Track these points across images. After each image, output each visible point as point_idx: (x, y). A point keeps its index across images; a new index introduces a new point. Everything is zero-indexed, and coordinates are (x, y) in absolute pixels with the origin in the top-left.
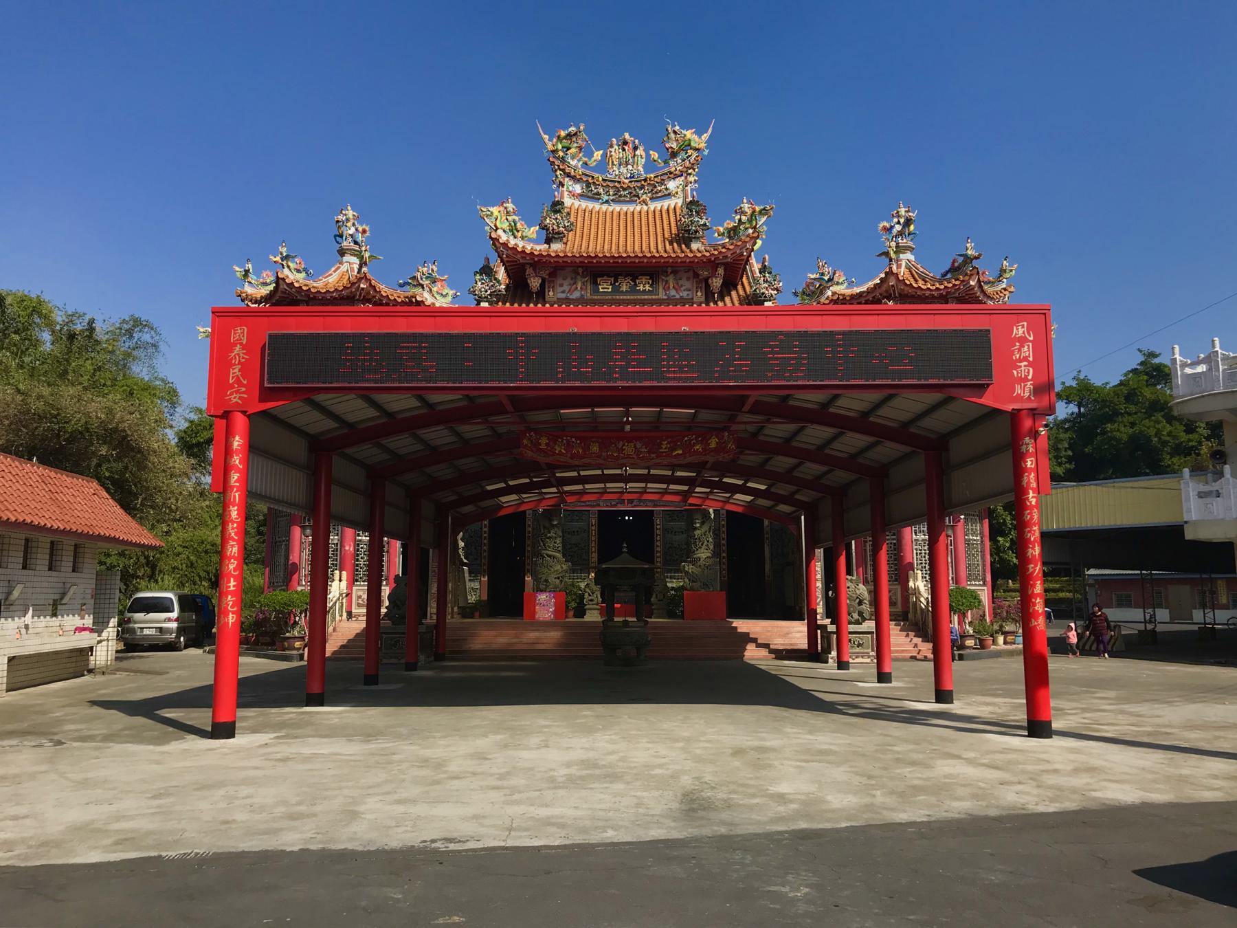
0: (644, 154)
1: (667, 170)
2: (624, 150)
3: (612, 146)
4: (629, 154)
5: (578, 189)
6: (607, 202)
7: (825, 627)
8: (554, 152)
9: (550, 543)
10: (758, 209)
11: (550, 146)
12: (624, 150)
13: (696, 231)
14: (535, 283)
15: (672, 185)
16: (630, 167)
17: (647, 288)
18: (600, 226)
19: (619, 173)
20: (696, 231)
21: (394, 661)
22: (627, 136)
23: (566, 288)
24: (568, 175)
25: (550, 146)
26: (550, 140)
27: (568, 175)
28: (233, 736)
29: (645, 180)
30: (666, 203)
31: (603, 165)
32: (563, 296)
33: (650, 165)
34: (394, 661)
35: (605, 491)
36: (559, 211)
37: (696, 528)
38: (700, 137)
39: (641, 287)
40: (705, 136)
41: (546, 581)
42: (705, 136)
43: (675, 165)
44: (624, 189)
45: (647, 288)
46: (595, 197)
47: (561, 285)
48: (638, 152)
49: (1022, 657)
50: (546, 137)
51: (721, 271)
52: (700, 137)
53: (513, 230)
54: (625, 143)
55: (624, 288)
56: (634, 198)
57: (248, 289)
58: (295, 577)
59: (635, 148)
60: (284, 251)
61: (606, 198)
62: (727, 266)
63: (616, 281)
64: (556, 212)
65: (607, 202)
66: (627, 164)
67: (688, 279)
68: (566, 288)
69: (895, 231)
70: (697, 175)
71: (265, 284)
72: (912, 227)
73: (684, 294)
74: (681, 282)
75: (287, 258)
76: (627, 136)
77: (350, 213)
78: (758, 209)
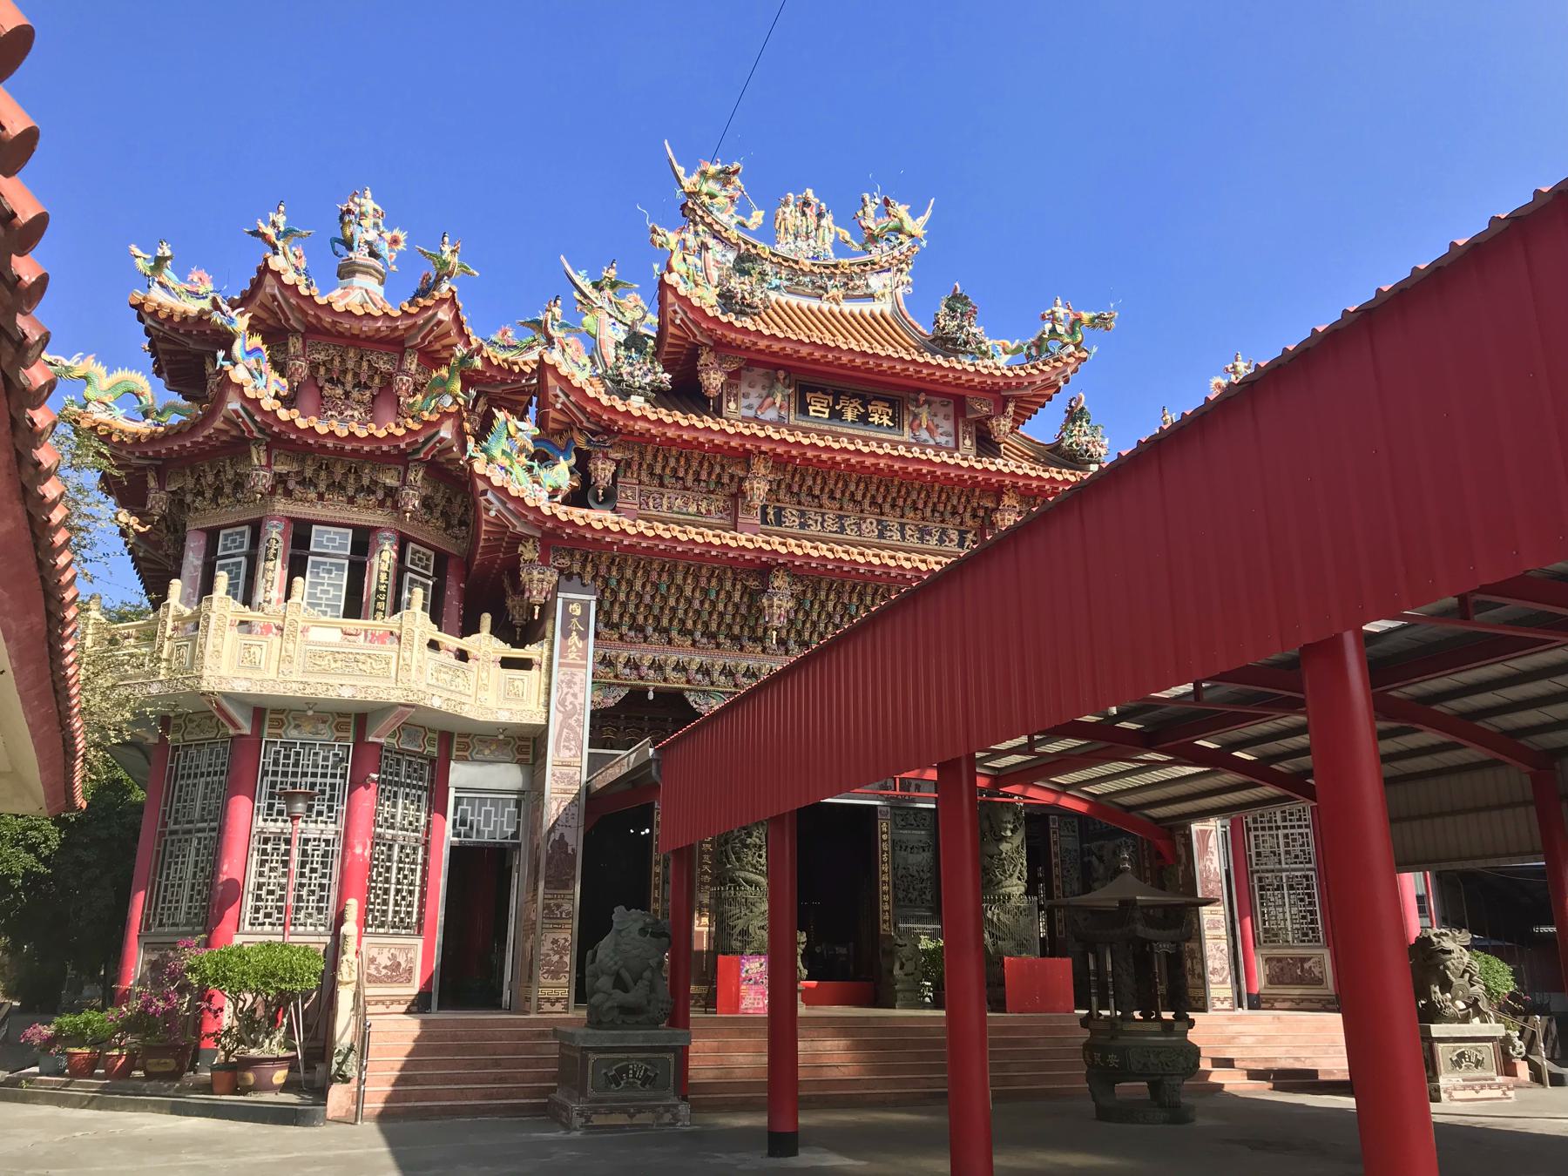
1: (866, 258)
2: (804, 214)
3: (786, 204)
4: (812, 221)
6: (777, 288)
7: (1520, 1038)
9: (749, 857)
10: (1086, 316)
12: (804, 214)
13: (966, 343)
14: (714, 380)
15: (876, 282)
16: (811, 242)
20: (966, 343)
21: (621, 1119)
22: (810, 193)
25: (688, 184)
26: (687, 175)
29: (836, 266)
30: (867, 307)
31: (768, 232)
32: (751, 413)
33: (840, 246)
34: (621, 1119)
37: (1004, 839)
38: (914, 218)
39: (876, 419)
40: (922, 220)
41: (745, 932)
42: (922, 220)
43: (878, 253)
44: (805, 274)
45: (886, 421)
47: (746, 396)
48: (824, 222)
49: (763, 1041)
52: (914, 218)
54: (806, 203)
55: (849, 415)
56: (819, 292)
57: (157, 295)
58: (231, 913)
59: (820, 215)
61: (776, 282)
63: (836, 402)
65: (777, 288)
67: (946, 417)
68: (755, 402)
70: (910, 274)
71: (196, 295)
74: (936, 421)
77: (369, 205)
78: (1086, 316)
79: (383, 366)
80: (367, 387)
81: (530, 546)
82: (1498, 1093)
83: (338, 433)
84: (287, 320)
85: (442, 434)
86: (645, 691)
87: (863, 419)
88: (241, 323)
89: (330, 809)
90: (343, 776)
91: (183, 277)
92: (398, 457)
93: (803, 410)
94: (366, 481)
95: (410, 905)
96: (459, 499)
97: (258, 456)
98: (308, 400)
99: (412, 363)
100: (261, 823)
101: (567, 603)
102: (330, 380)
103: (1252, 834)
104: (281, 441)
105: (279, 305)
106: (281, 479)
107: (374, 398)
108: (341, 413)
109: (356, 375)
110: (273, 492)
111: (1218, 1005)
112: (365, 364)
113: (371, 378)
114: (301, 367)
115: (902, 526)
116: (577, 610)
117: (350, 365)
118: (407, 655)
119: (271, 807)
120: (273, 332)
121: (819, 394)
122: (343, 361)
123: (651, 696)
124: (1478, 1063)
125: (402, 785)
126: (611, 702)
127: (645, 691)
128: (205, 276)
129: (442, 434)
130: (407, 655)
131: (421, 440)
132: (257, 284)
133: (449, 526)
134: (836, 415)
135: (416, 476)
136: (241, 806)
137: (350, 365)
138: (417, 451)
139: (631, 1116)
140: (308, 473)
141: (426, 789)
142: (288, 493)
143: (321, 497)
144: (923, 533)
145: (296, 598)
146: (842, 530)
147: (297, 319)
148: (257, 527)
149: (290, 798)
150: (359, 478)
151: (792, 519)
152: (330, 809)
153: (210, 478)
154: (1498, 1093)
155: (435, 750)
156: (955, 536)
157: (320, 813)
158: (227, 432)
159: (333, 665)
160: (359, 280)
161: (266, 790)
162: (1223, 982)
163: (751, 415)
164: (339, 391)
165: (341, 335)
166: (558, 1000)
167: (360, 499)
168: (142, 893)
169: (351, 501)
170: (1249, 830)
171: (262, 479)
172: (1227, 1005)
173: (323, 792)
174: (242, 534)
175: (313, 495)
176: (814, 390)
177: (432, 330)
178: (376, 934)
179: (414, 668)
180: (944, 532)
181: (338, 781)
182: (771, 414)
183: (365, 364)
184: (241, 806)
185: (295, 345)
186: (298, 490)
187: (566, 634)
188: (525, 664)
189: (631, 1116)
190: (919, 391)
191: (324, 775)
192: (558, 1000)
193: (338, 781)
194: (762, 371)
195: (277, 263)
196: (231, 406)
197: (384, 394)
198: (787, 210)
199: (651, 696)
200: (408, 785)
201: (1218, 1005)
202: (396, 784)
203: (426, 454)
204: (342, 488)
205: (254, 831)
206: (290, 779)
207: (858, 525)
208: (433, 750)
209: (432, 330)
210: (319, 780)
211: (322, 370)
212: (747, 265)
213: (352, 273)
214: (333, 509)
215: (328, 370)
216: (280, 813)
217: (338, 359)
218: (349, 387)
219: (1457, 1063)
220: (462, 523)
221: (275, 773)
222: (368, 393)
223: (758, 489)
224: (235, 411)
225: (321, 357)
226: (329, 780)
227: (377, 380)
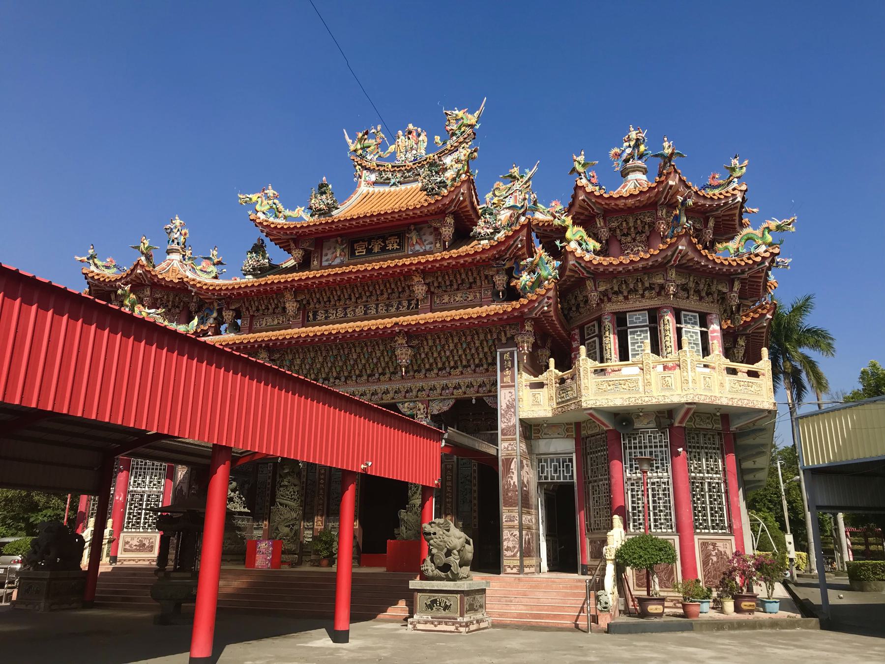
0: (426, 140)
2: (409, 138)
4: (412, 142)
5: (373, 177)
6: (394, 184)
8: (355, 151)
11: (352, 148)
12: (409, 138)
16: (414, 152)
17: (396, 246)
18: (367, 197)
19: (405, 158)
22: (411, 126)
23: (329, 256)
24: (365, 168)
26: (353, 143)
27: (365, 168)
28: (499, 574)
35: (596, 439)
36: (325, 193)
39: (390, 247)
44: (408, 171)
45: (396, 246)
46: (386, 182)
48: (421, 138)
50: (349, 141)
51: (450, 220)
53: (275, 212)
54: (410, 133)
55: (376, 250)
59: (419, 135)
60: (91, 251)
61: (393, 181)
62: (456, 215)
64: (322, 193)
65: (394, 184)
66: (412, 149)
67: (431, 234)
69: (625, 156)
72: (642, 148)
73: (428, 248)
74: (424, 238)
75: (92, 257)
76: (411, 126)
77: (178, 222)
79: (648, 220)
80: (642, 232)
81: (529, 323)
82: (452, 628)
83: (624, 262)
84: (593, 210)
85: (680, 247)
86: (470, 399)
87: (383, 250)
88: (569, 221)
89: (663, 464)
90: (666, 446)
91: (547, 206)
92: (661, 267)
93: (352, 254)
94: (647, 285)
95: (722, 516)
96: (703, 281)
97: (590, 284)
98: (614, 248)
99: (662, 213)
100: (628, 475)
101: (502, 355)
102: (624, 235)
103: (628, 451)
104: (597, 274)
105: (588, 204)
106: (605, 293)
107: (648, 237)
108: (632, 250)
109: (635, 228)
110: (602, 301)
111: (509, 570)
112: (639, 221)
113: (644, 227)
114: (604, 233)
115: (377, 305)
116: (507, 356)
117: (171, 299)
118: (648, 377)
119: (631, 466)
120: (585, 220)
121: (361, 243)
122: (627, 223)
123: (474, 401)
124: (446, 608)
125: (702, 448)
126: (446, 408)
127: (470, 399)
128: (558, 203)
129: (680, 247)
130: (648, 377)
131: (670, 253)
132: (575, 197)
133: (701, 298)
134: (369, 252)
135: (673, 274)
136: (616, 465)
137: (631, 224)
138: (670, 261)
139: (435, 626)
140: (616, 289)
141: (718, 449)
142: (609, 300)
143: (626, 298)
144: (388, 306)
145: (685, 346)
146: (346, 314)
147: (598, 208)
148: (599, 320)
149: (641, 461)
150: (643, 284)
151: (321, 316)
152: (663, 464)
153: (573, 301)
154: (452, 628)
155: (720, 426)
156: (405, 304)
157: (657, 468)
158: (573, 276)
159: (609, 388)
160: (632, 176)
161: (628, 457)
162: (514, 556)
163: (334, 265)
164: (629, 239)
165: (622, 210)
166: (514, 567)
167: (647, 293)
168: (582, 512)
169: (643, 296)
170: (625, 448)
171: (594, 297)
172: (515, 570)
173: (656, 456)
174: (594, 326)
175: (621, 298)
176: (357, 242)
177: (668, 192)
178: (700, 534)
179: (690, 381)
180: (400, 303)
181: (664, 449)
182: (337, 261)
183: (639, 221)
184: (616, 465)
185: (600, 223)
186: (614, 298)
187: (503, 369)
188: (541, 385)
189: (435, 626)
190: (409, 225)
191: (656, 447)
192: (514, 567)
193: (664, 449)
194: (334, 240)
195: (583, 182)
196: (571, 262)
197: (650, 235)
198: (399, 140)
199: (474, 401)
200: (706, 448)
201: (509, 570)
202: (698, 447)
203: (675, 261)
204: (635, 291)
205: (625, 480)
206: (659, 449)
207: (354, 311)
208: (719, 426)
209: (668, 192)
210: (653, 449)
211: (618, 231)
212: (323, 190)
213: (628, 174)
214: (635, 303)
215: (621, 230)
216: (637, 468)
217: (624, 223)
218: (633, 235)
219: (430, 606)
220: (708, 294)
221: (137, 468)
222: (644, 235)
223: (420, 290)
224: (573, 265)
225: (614, 224)
226: (659, 449)
227: (647, 227)
